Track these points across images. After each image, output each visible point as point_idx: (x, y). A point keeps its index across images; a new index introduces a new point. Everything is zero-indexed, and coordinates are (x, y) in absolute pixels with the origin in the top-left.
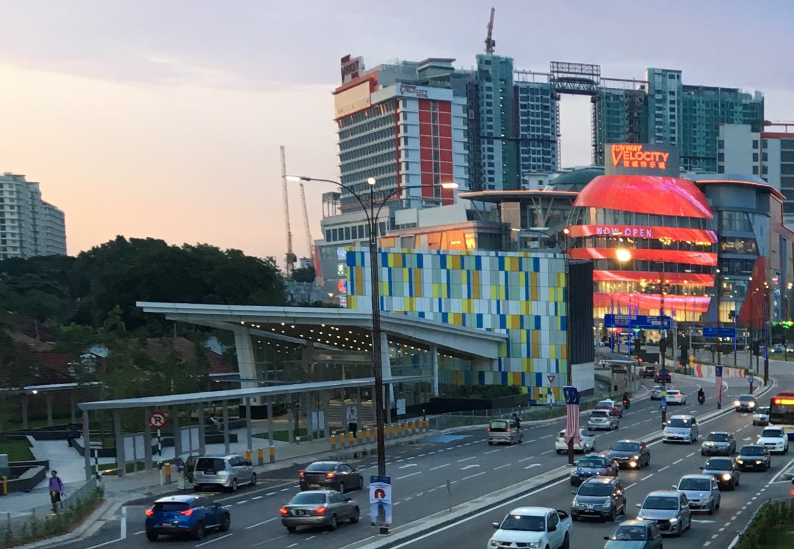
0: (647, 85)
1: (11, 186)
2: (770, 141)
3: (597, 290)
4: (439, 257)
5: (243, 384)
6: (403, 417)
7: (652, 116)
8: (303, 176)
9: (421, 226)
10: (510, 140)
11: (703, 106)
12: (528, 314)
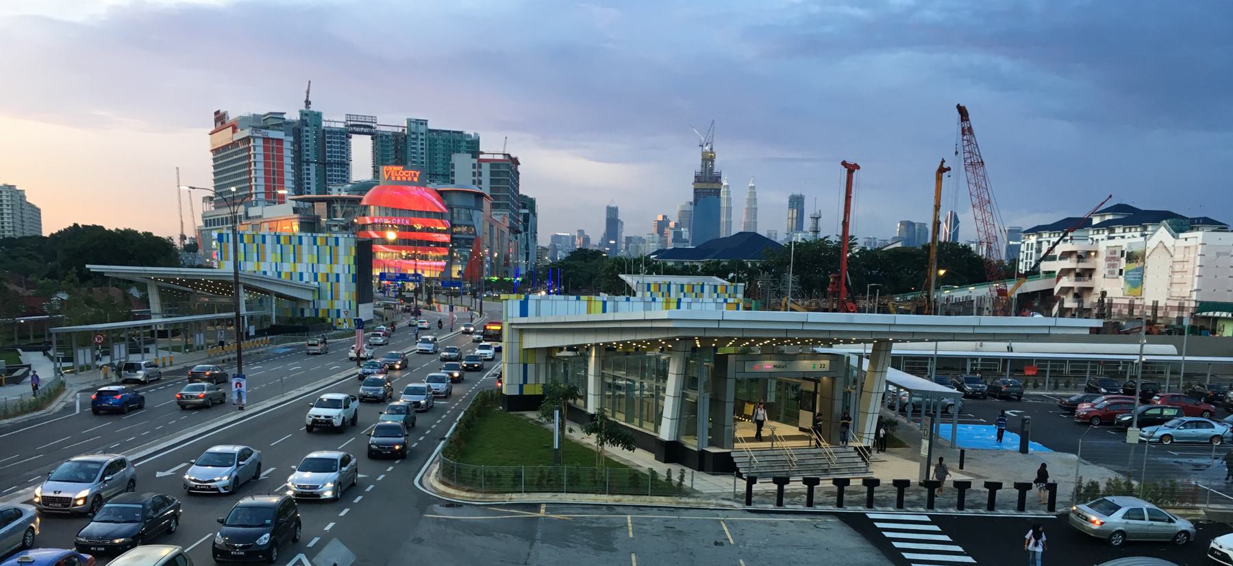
0: (406, 129)
2: (483, 164)
3: (375, 257)
4: (275, 237)
5: (152, 316)
6: (253, 337)
7: (409, 148)
10: (320, 163)
11: (441, 142)
12: (331, 272)
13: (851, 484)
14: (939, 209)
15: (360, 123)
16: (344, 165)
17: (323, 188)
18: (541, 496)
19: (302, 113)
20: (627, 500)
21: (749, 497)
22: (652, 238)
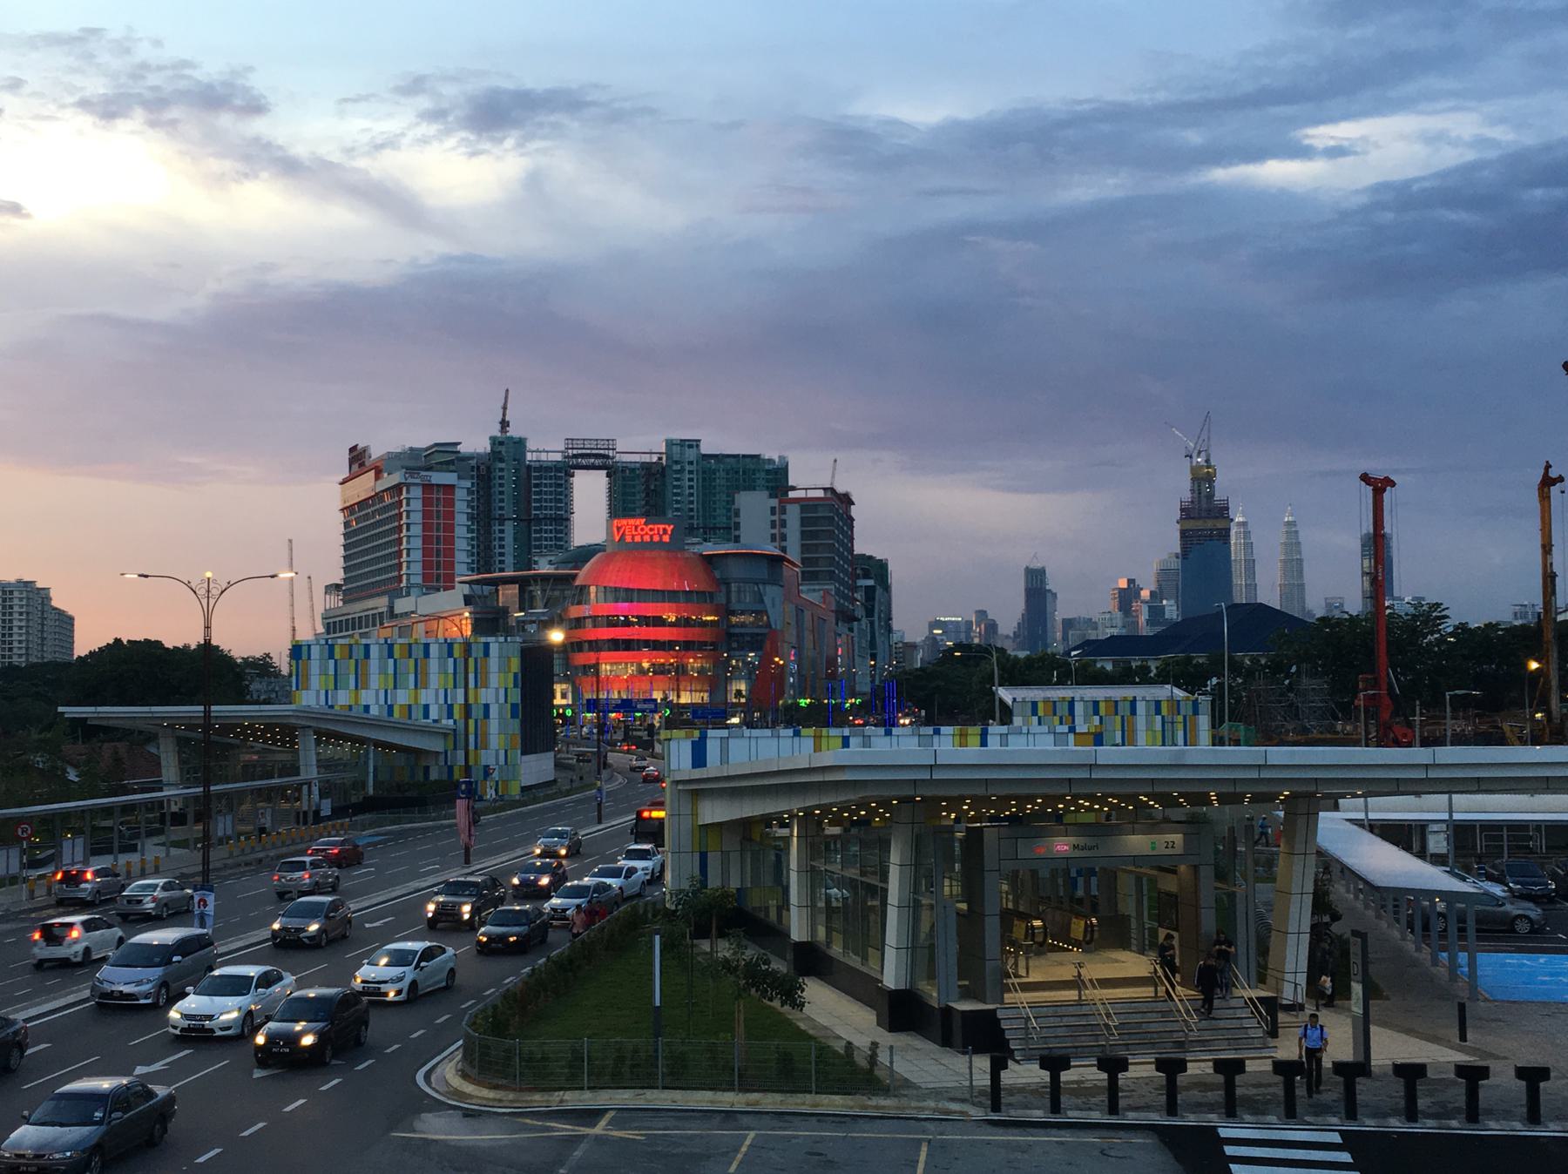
0: (664, 457)
1: (21, 592)
4: (386, 646)
5: (165, 788)
6: (329, 818)
7: (670, 488)
8: (140, 573)
9: (419, 612)
11: (723, 474)
12: (356, 704)
13: (1247, 1069)
14: (1551, 550)
15: (589, 451)
16: (562, 520)
17: (525, 561)
18: (618, 1097)
19: (493, 440)
20: (770, 1101)
21: (995, 1094)
22: (1111, 619)
